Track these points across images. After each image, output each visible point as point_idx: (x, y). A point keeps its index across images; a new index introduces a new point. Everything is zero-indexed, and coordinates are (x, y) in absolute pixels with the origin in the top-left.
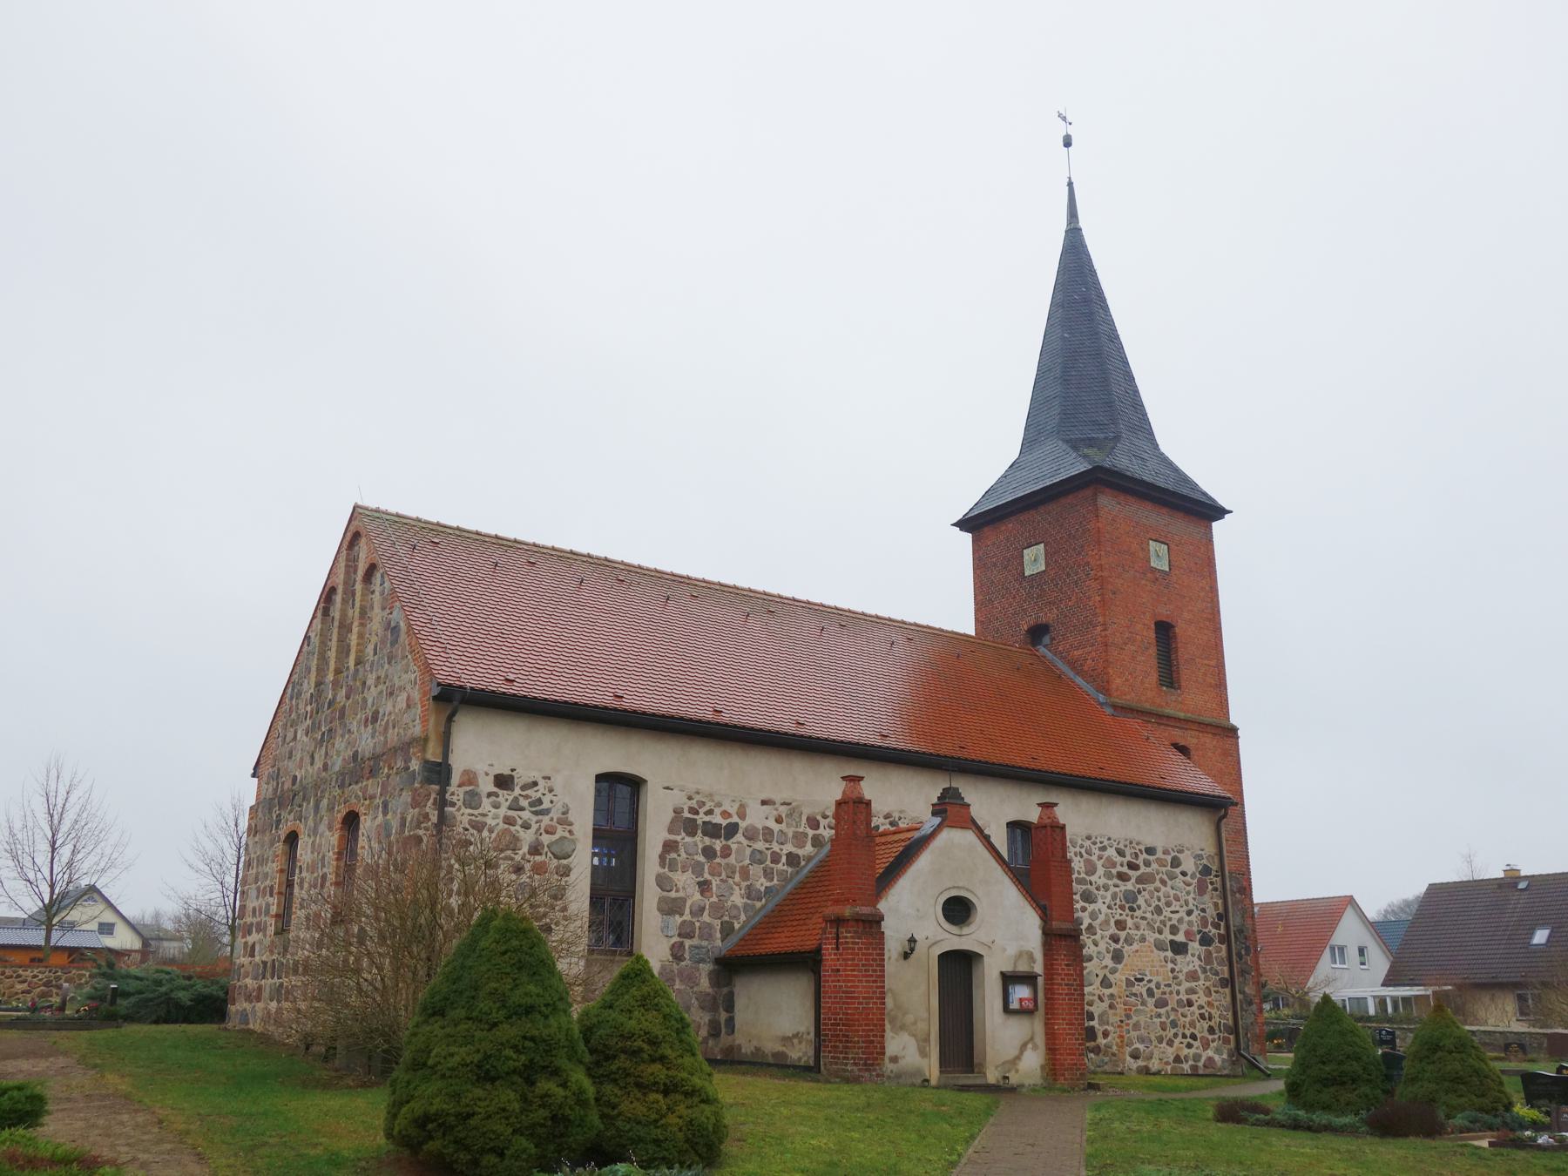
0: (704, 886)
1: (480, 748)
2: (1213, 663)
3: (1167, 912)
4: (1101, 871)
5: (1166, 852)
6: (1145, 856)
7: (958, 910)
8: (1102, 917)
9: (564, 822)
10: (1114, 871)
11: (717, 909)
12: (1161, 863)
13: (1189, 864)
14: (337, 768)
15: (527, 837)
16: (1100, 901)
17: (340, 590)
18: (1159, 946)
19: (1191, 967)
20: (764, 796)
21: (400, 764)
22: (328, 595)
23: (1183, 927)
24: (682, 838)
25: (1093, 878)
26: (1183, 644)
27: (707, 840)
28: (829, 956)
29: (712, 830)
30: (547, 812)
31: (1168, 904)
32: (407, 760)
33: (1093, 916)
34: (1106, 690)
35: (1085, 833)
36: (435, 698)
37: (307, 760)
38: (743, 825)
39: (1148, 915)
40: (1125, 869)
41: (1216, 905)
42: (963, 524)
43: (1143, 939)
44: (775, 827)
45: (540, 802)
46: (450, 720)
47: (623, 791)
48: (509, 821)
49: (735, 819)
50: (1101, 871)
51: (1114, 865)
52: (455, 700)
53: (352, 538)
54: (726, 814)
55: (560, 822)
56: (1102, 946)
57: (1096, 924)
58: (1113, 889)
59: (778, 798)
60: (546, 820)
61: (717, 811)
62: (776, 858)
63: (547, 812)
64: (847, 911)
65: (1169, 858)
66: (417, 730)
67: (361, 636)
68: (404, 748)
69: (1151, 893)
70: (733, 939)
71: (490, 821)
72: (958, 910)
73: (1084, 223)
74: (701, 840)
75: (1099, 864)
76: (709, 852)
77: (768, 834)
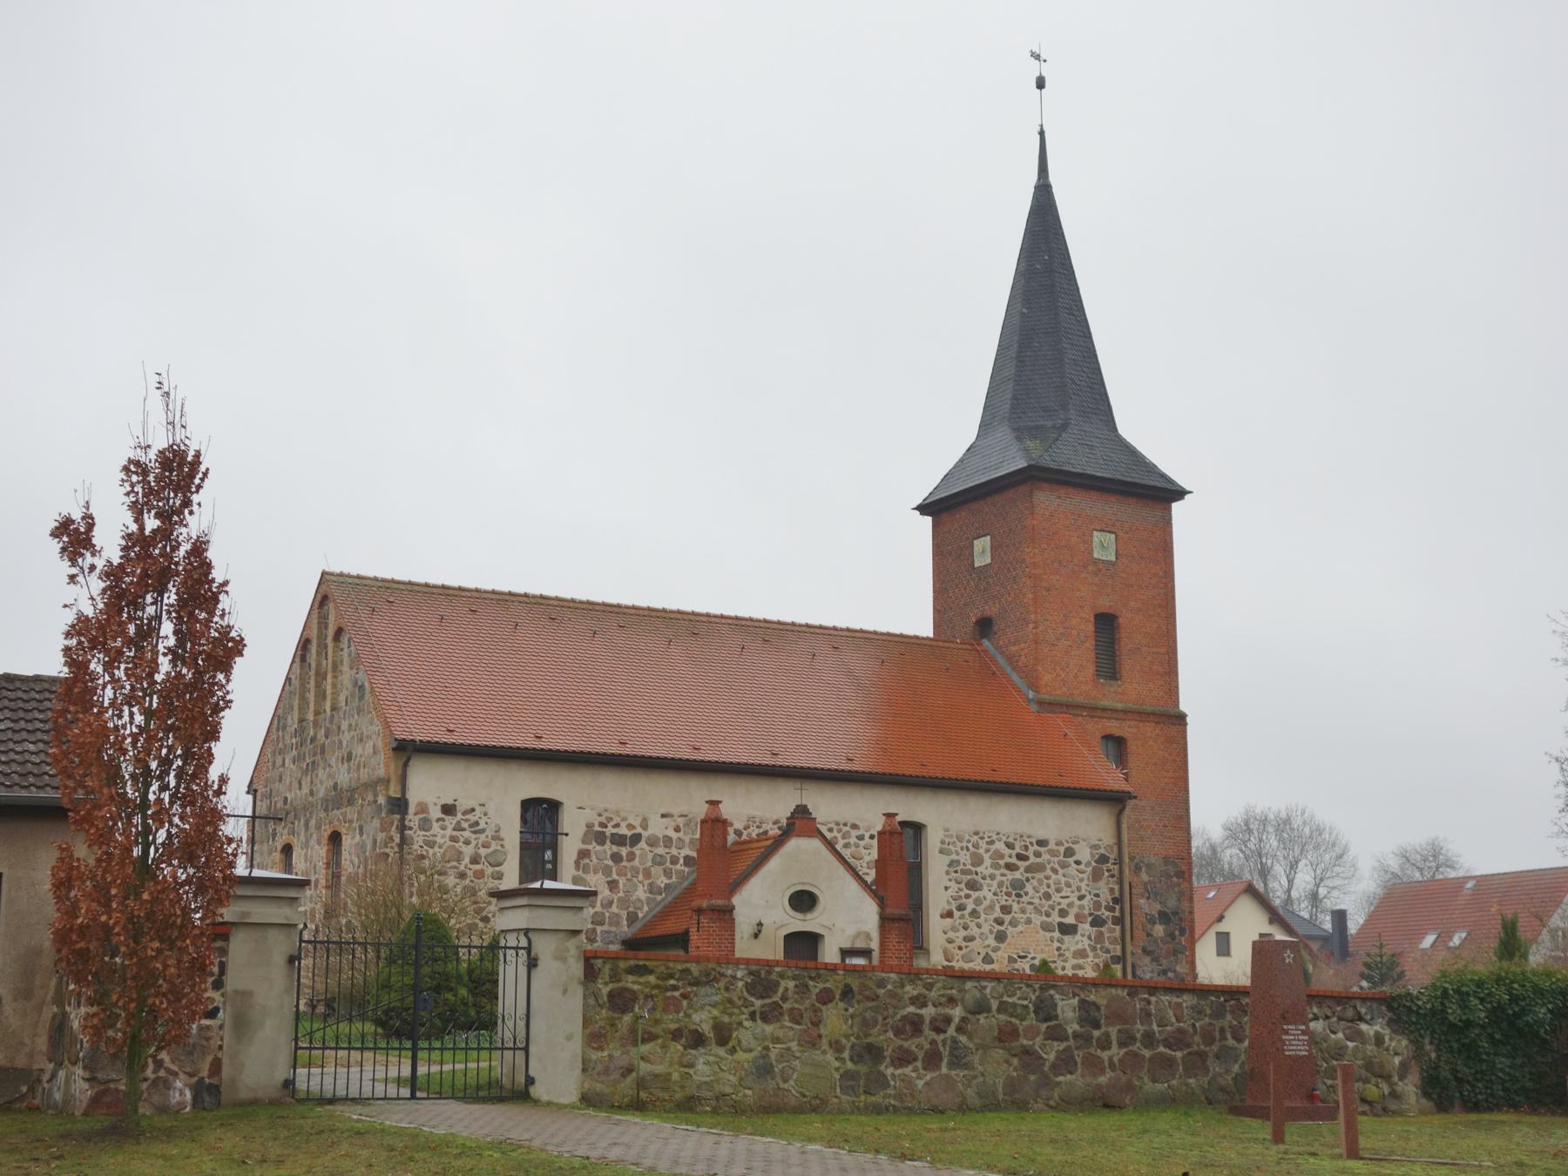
0: (613, 885)
1: (429, 785)
2: (1163, 650)
3: (1056, 897)
4: (988, 862)
5: (1059, 843)
6: (1036, 847)
7: (804, 901)
8: (986, 903)
9: (497, 838)
10: (1002, 862)
11: (624, 902)
12: (1053, 853)
13: (1084, 853)
14: (321, 794)
15: (468, 851)
17: (314, 642)
18: (1046, 927)
19: (1080, 946)
20: (664, 811)
21: (370, 797)
22: (304, 645)
23: (1073, 911)
24: (594, 847)
25: (979, 869)
26: (1132, 632)
27: (615, 849)
28: (694, 936)
29: (619, 840)
30: (483, 831)
31: (1058, 890)
32: (376, 795)
33: (978, 902)
34: (1034, 686)
35: (973, 829)
36: (394, 749)
37: (296, 785)
38: (645, 834)
39: (1036, 901)
40: (1014, 860)
41: (1112, 890)
42: (923, 509)
43: (1029, 921)
44: (674, 835)
45: (477, 823)
46: (406, 765)
48: (454, 839)
49: (639, 830)
51: (1002, 856)
52: (407, 750)
53: (322, 600)
54: (630, 827)
55: (494, 838)
56: (986, 929)
57: (980, 909)
58: (999, 878)
59: (675, 811)
60: (482, 837)
61: (623, 824)
62: (674, 861)
63: (483, 831)
64: (705, 904)
65: (1062, 849)
66: (381, 772)
67: (334, 686)
68: (373, 785)
69: (1040, 881)
70: (638, 925)
71: (439, 840)
72: (804, 901)
73: (1053, 178)
74: (609, 849)
75: (986, 857)
76: (616, 858)
77: (668, 841)
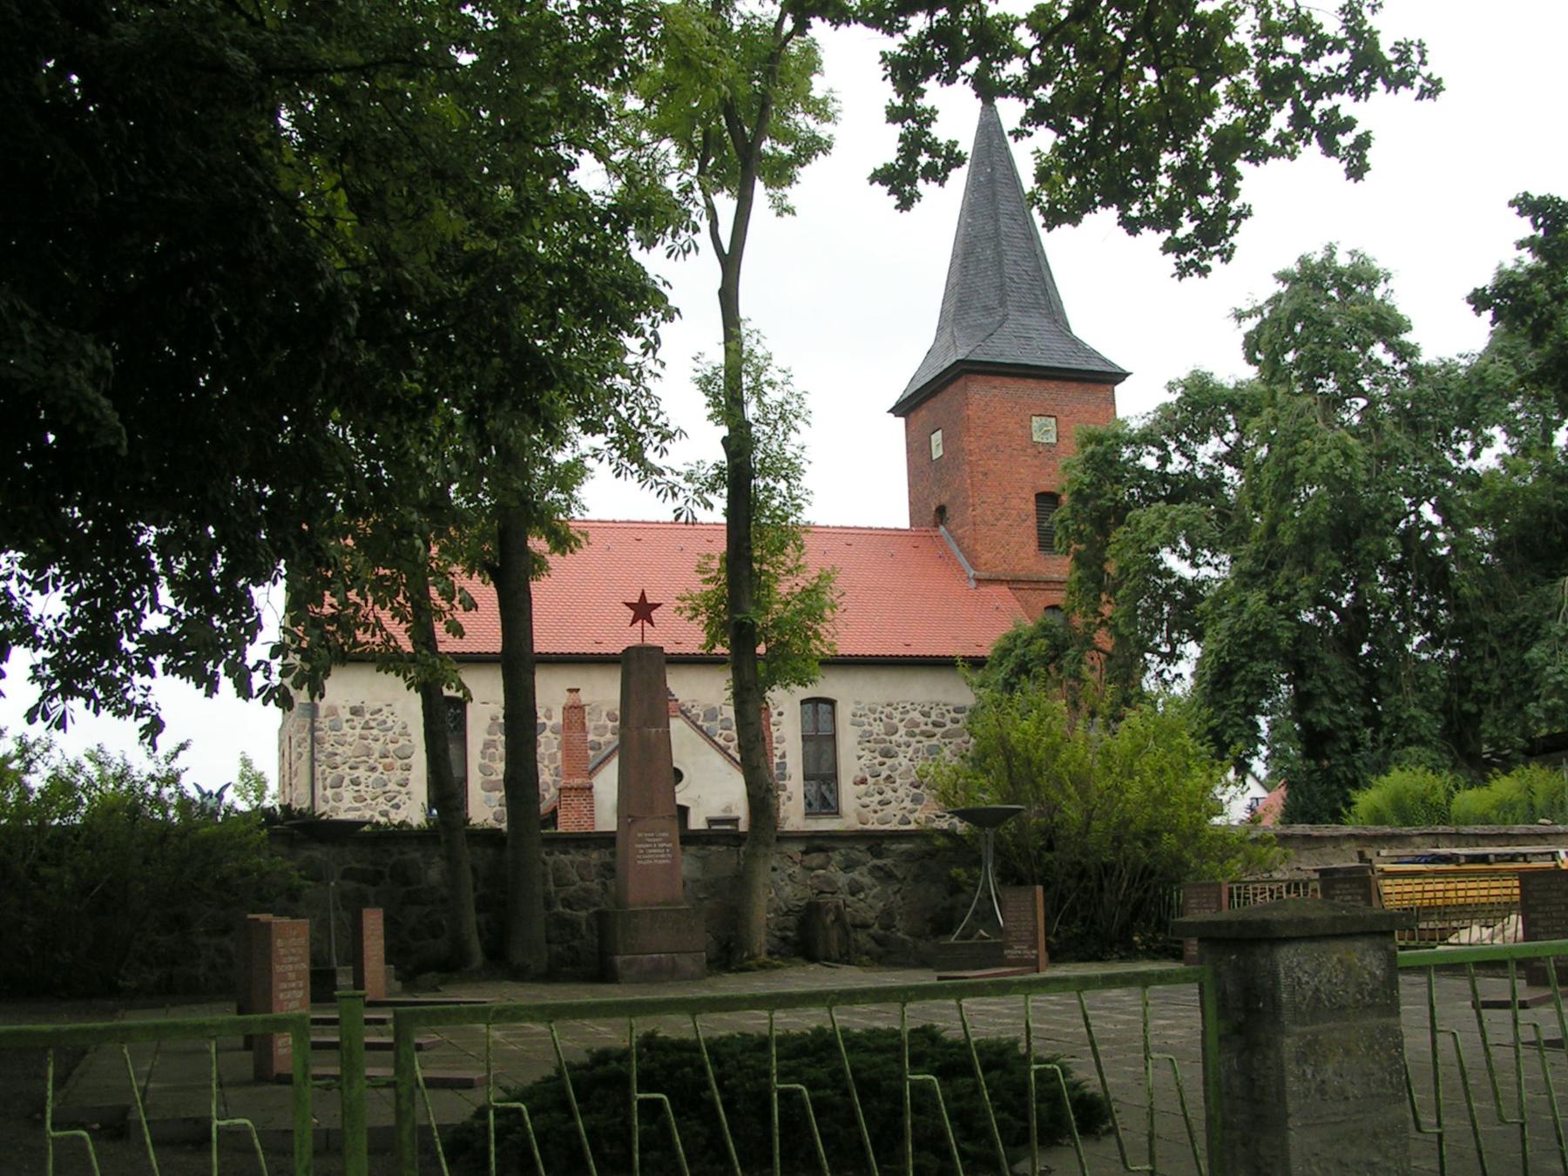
4: (902, 731)
15: (377, 747)
16: (901, 755)
25: (893, 738)
35: (884, 701)
42: (897, 410)
45: (385, 722)
47: (823, 707)
50: (902, 731)
56: (901, 793)
58: (914, 745)
